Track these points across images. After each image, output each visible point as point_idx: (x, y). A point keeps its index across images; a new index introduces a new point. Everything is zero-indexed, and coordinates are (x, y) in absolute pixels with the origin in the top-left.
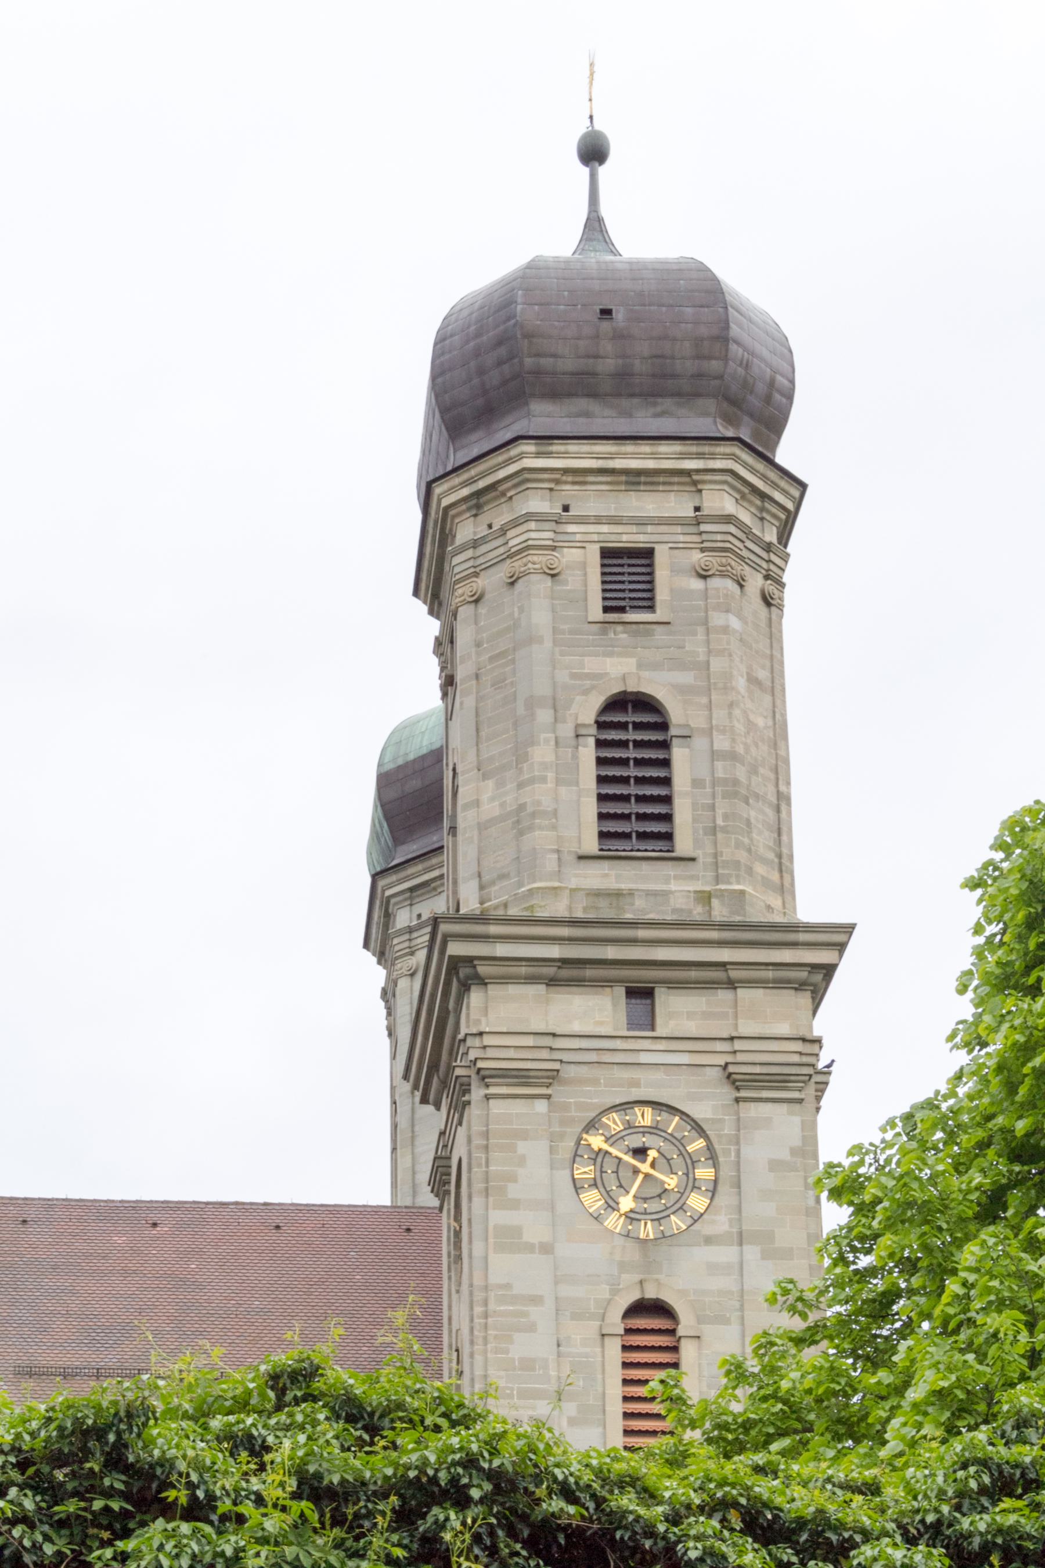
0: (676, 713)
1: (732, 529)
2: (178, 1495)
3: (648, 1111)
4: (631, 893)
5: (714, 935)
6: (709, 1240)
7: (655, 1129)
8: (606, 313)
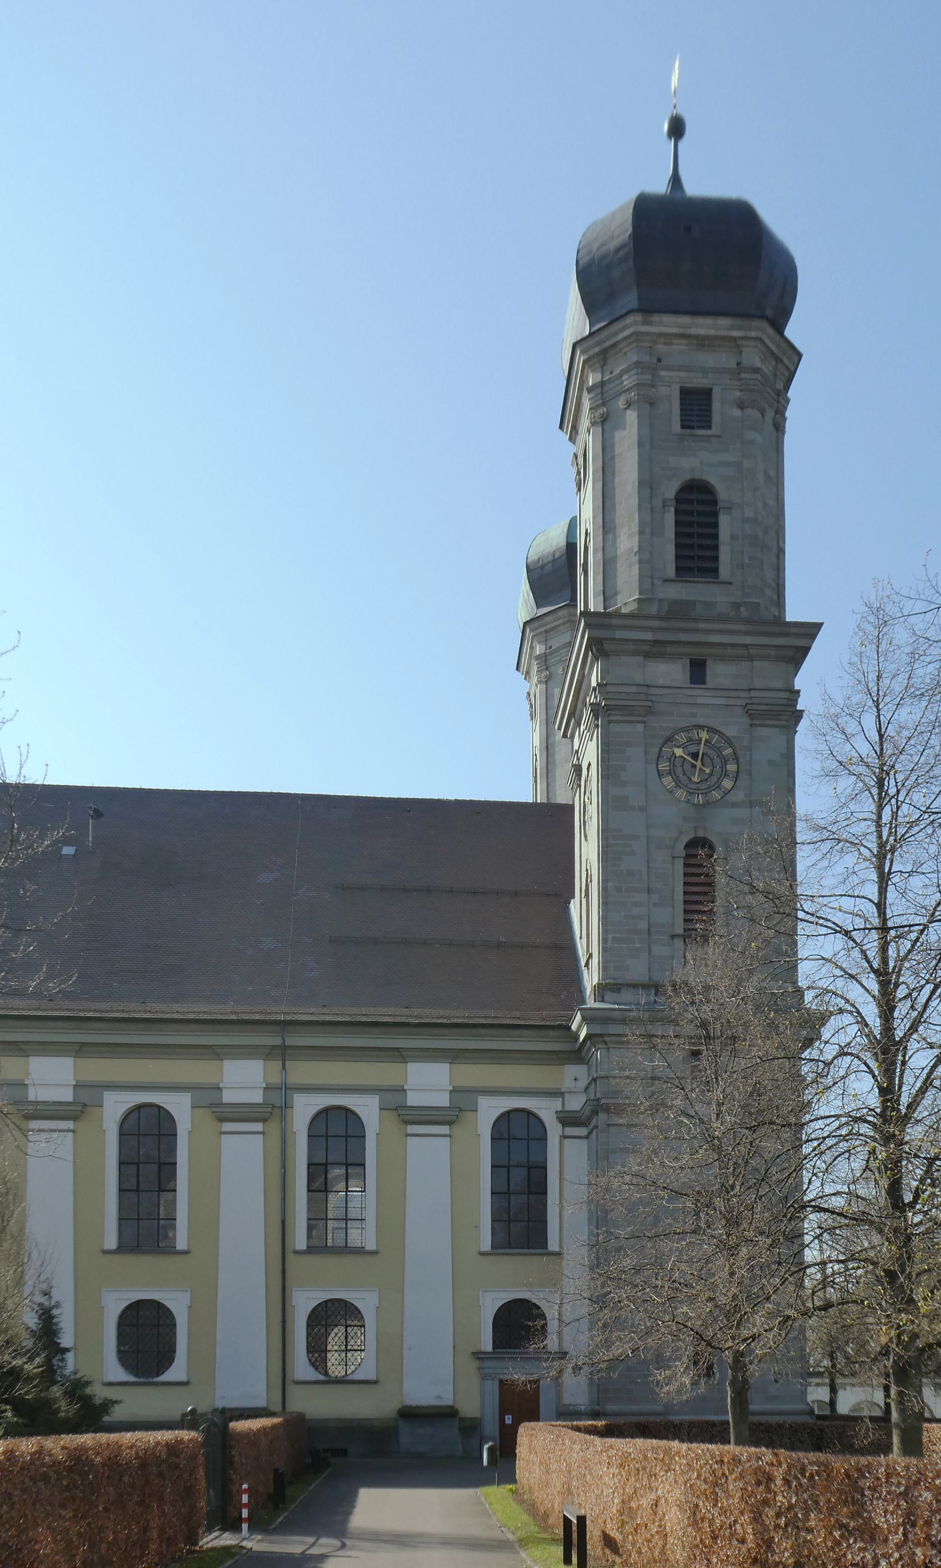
0: (722, 493)
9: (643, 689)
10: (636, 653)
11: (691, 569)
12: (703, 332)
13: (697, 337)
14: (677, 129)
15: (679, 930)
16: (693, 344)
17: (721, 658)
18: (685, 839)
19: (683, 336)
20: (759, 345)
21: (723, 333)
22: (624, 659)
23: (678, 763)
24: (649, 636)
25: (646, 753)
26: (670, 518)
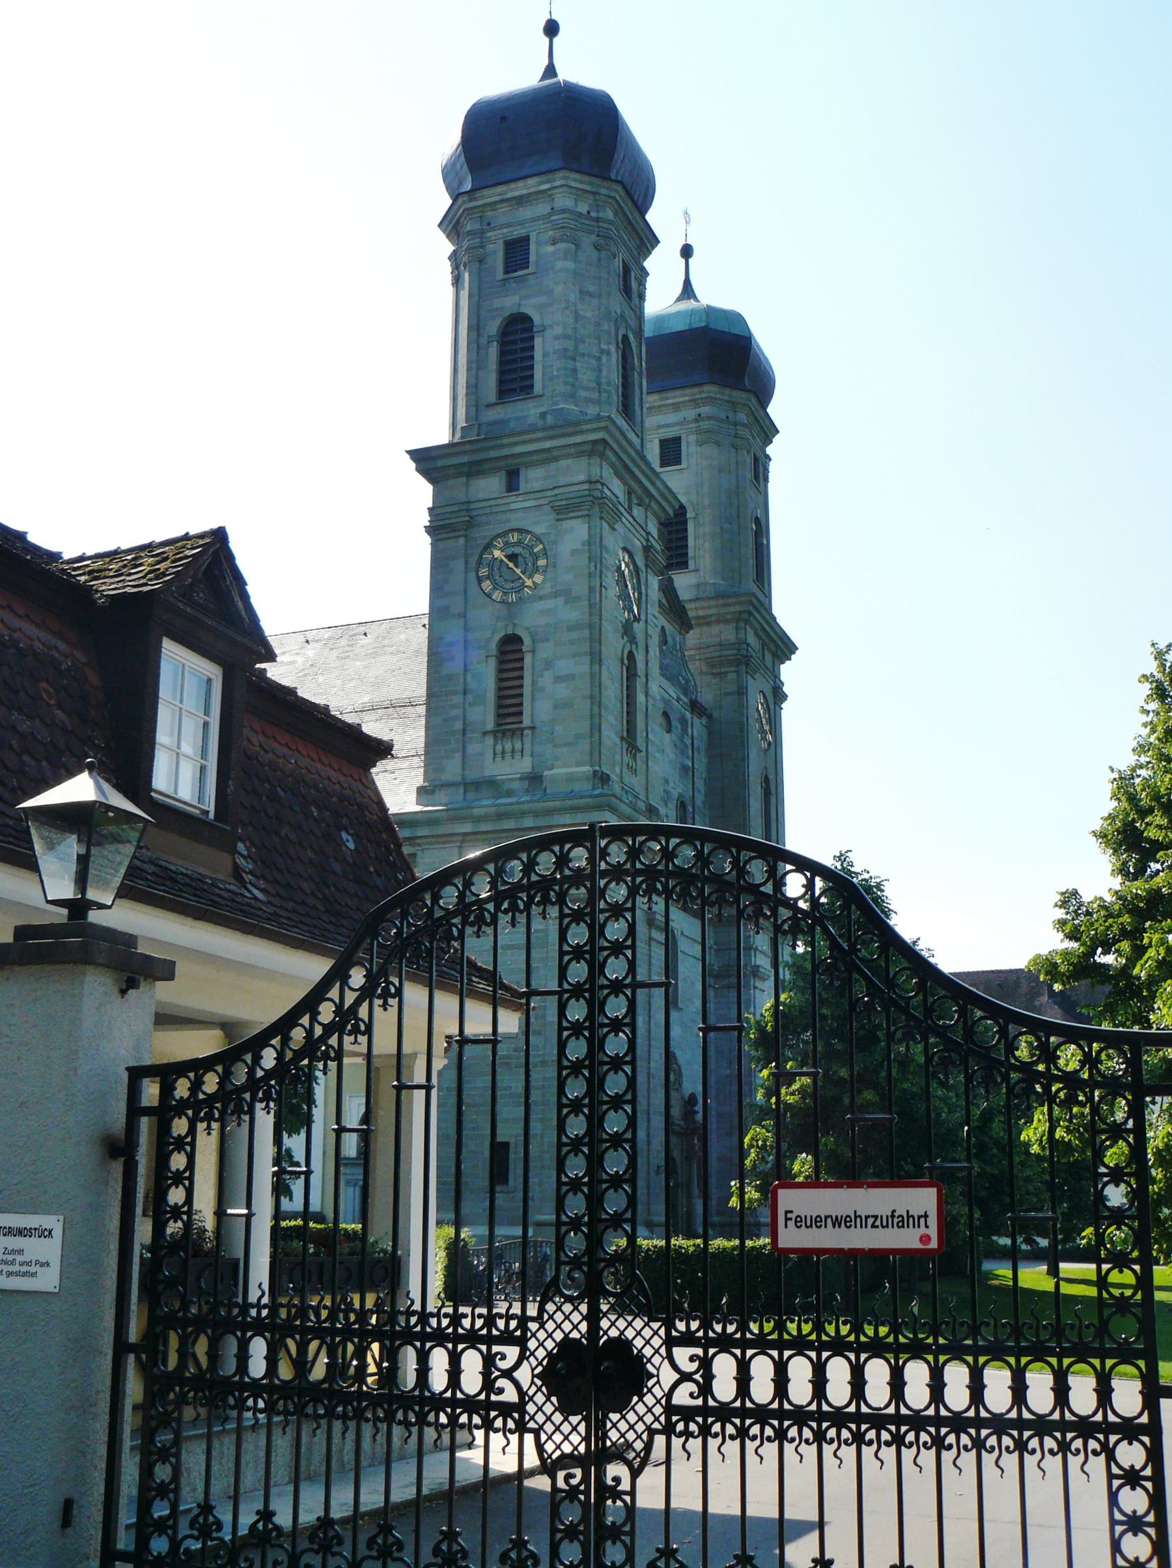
0: (537, 320)
1: (566, 215)
2: (698, 727)
3: (516, 534)
4: (509, 420)
5: (540, 435)
6: (541, 598)
7: (519, 543)
8: (503, 118)
9: (465, 507)
10: (459, 475)
11: (515, 389)
12: (516, 194)
13: (515, 198)
14: (551, 29)
15: (490, 726)
16: (548, 200)
17: (528, 465)
18: (497, 637)
19: (502, 201)
20: (565, 189)
21: (533, 190)
22: (451, 482)
23: (497, 565)
24: (465, 459)
25: (466, 563)
26: (493, 351)
